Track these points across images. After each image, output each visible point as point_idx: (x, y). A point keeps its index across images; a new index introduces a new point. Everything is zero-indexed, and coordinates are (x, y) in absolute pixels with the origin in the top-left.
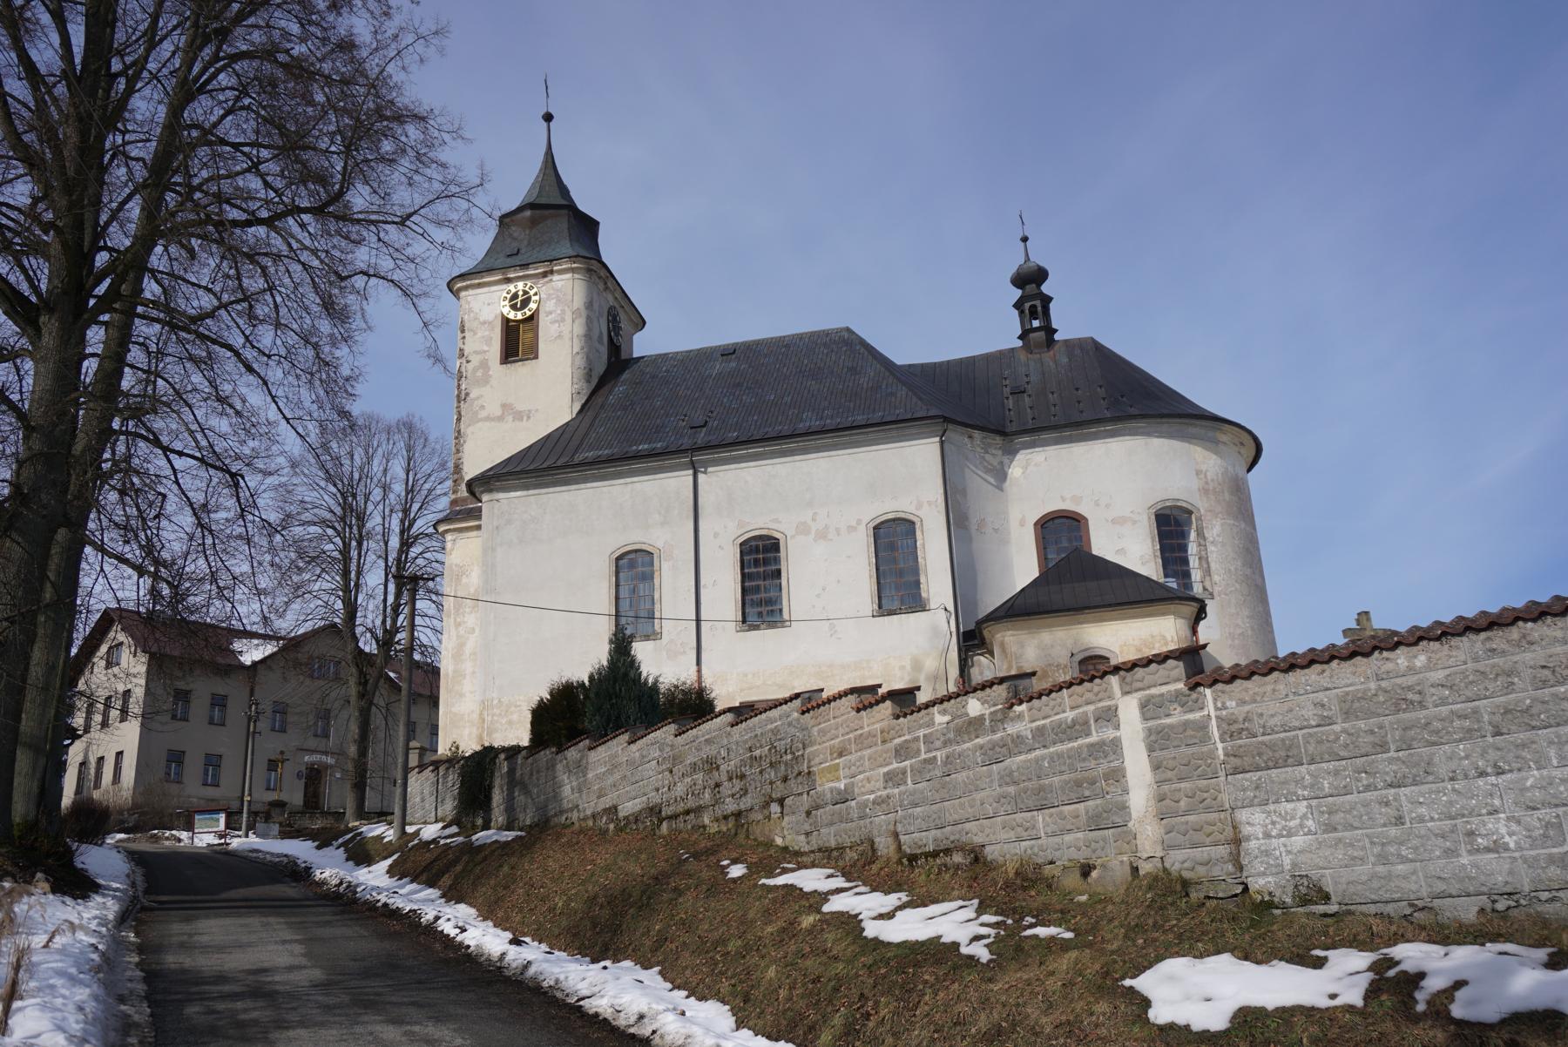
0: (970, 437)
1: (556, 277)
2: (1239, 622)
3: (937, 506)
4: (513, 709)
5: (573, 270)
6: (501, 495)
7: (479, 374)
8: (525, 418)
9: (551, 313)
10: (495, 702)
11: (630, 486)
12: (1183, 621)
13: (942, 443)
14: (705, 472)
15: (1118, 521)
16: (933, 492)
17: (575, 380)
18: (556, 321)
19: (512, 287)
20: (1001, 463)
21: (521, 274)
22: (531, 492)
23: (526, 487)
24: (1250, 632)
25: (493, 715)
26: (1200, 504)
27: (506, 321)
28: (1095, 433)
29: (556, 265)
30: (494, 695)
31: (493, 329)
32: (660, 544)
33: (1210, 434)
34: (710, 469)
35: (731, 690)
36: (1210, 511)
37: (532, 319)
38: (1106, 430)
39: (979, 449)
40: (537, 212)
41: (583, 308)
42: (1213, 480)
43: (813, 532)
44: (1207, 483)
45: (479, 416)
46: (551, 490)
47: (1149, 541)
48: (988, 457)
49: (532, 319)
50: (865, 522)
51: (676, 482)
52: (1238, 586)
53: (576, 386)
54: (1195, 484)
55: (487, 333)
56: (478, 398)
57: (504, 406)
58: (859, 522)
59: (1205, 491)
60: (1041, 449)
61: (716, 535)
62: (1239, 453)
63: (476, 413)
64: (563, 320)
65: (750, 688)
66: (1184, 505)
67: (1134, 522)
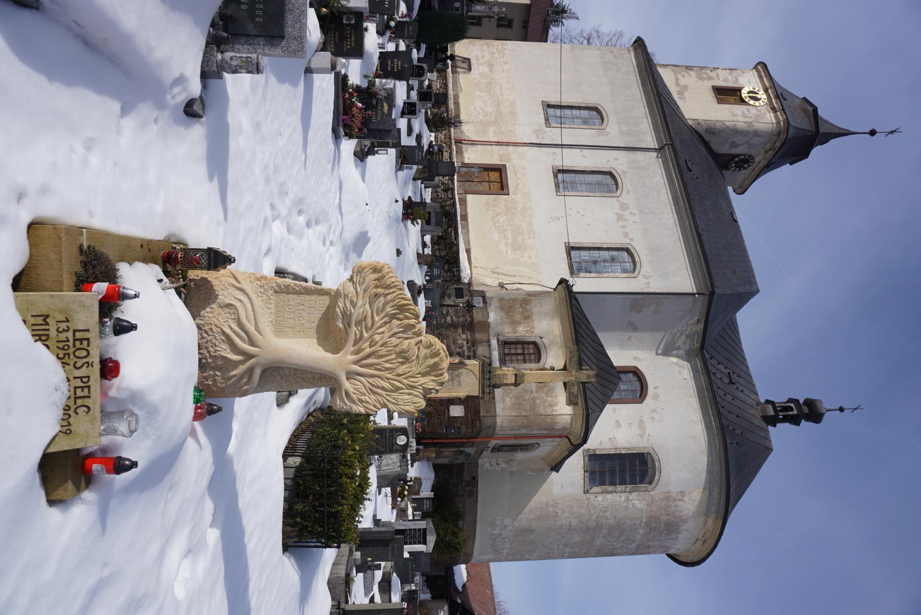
0: (698, 321)
1: (772, 115)
2: (566, 515)
3: (646, 288)
4: (501, 55)
5: (778, 123)
6: (632, 54)
7: (704, 76)
8: (680, 96)
9: (749, 111)
10: (506, 47)
11: (645, 116)
12: (569, 421)
13: (693, 294)
14: (657, 157)
15: (641, 424)
16: (656, 286)
17: (707, 122)
18: (743, 114)
19: (762, 92)
20: (679, 349)
21: (771, 96)
22: (636, 69)
23: (638, 66)
24: (559, 523)
25: (498, 46)
26: (657, 491)
27: (739, 90)
28: (708, 414)
29: (781, 113)
30: (509, 47)
31: (733, 83)
32: (608, 130)
33: (713, 509)
34: (660, 160)
35: (514, 161)
36: (652, 500)
37: (742, 101)
38: (711, 422)
39: (689, 330)
40: (812, 114)
41: (754, 128)
42: (676, 506)
43: (622, 213)
44: (674, 500)
45: (678, 75)
46: (638, 78)
47: (627, 445)
48: (683, 337)
49: (742, 101)
50: (631, 243)
51: (650, 141)
52: (594, 517)
53: (703, 122)
54: (674, 489)
55: (730, 80)
56: (689, 74)
57: (686, 87)
58: (632, 240)
59: (668, 497)
60: (692, 376)
61: (616, 159)
62: (697, 540)
63: (680, 73)
64: (745, 117)
65: (515, 171)
66: (657, 477)
67: (641, 436)
